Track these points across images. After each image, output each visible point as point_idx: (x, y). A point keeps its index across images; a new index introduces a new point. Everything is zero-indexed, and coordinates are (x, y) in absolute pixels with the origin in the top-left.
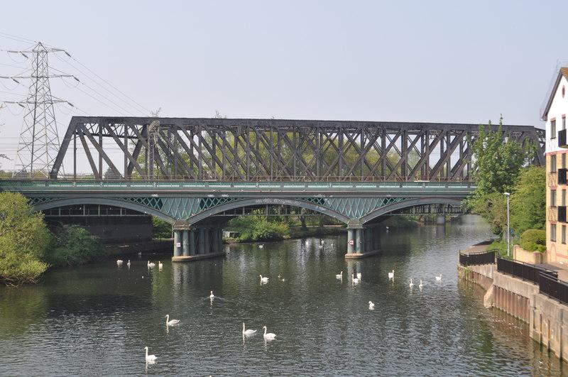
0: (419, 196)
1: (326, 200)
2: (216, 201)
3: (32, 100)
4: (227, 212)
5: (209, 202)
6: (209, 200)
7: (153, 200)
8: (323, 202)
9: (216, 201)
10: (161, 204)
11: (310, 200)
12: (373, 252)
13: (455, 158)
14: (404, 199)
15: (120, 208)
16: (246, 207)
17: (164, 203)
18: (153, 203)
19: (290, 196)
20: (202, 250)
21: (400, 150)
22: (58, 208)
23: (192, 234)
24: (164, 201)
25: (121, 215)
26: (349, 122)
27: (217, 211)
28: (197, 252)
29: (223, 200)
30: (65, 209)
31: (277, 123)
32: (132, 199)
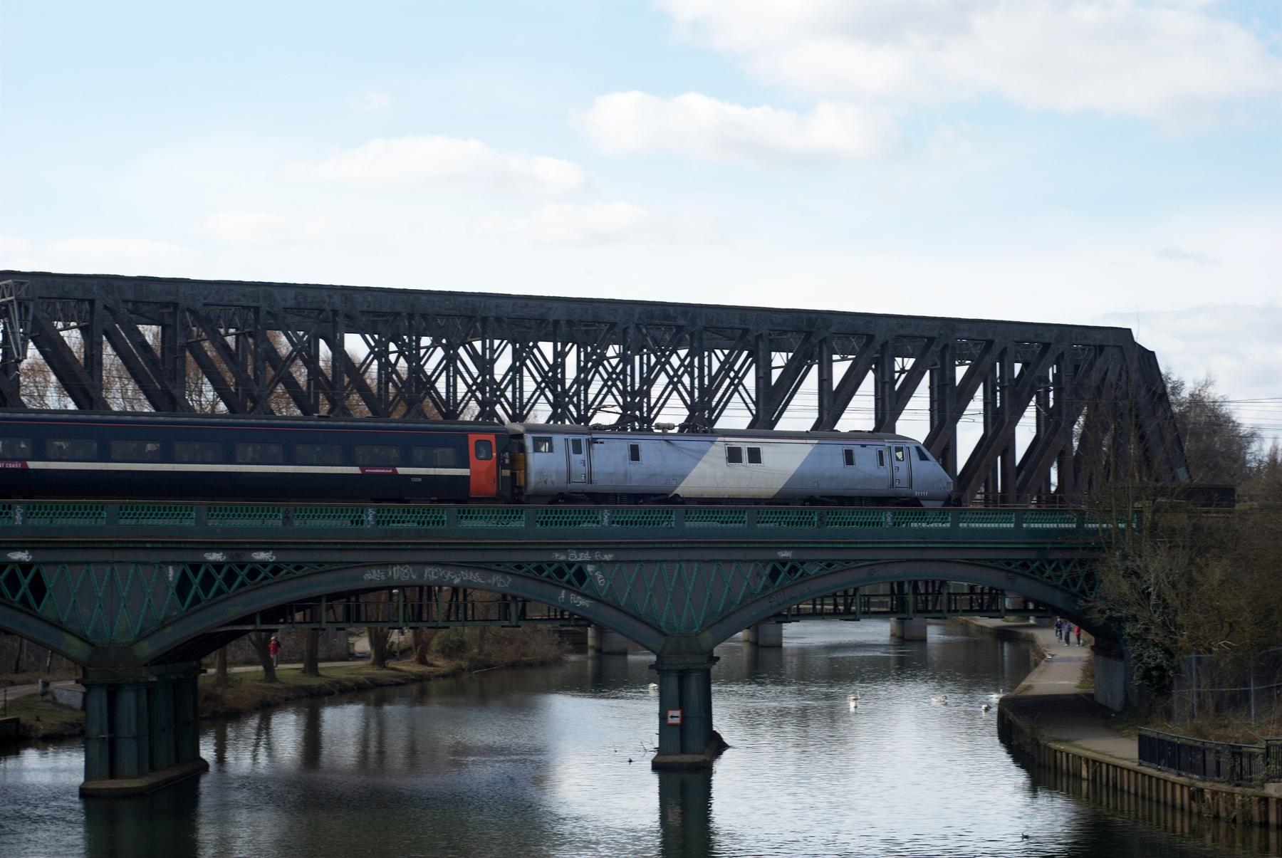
1: (590, 568)
2: (230, 578)
5: (207, 581)
7: (13, 572)
8: (581, 575)
9: (230, 578)
10: (38, 588)
11: (540, 569)
13: (1025, 432)
14: (298, 568)
19: (477, 557)
24: (51, 578)
29: (253, 574)
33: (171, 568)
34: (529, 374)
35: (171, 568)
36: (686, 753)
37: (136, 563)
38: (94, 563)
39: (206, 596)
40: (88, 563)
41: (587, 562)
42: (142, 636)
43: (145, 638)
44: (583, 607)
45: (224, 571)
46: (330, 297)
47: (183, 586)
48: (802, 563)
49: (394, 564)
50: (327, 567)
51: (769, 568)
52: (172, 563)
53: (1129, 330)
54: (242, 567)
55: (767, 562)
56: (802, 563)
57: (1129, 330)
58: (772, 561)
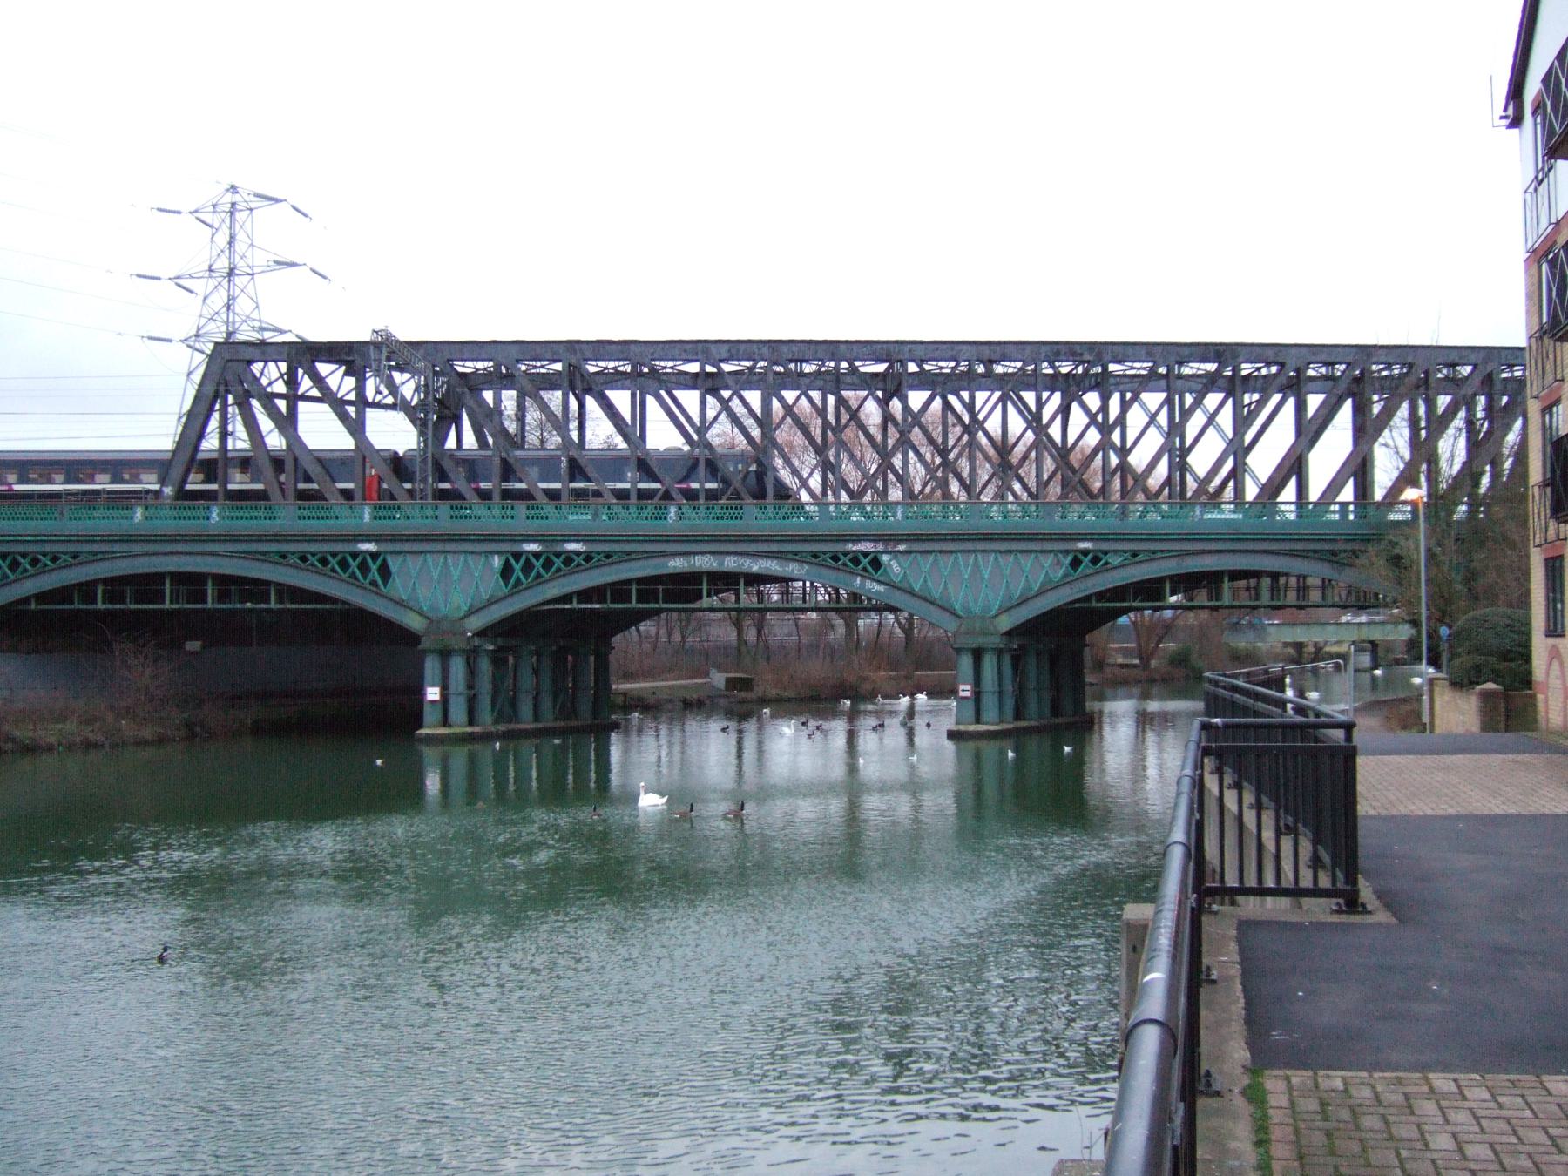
0: (1177, 546)
1: (885, 558)
2: (548, 564)
3: (222, 264)
4: (1100, 596)
5: (527, 568)
6: (528, 561)
7: (364, 560)
8: (876, 564)
9: (548, 564)
10: (385, 572)
12: (469, 729)
14: (1135, 554)
15: (268, 583)
16: (639, 581)
17: (393, 569)
18: (364, 567)
19: (774, 547)
20: (1032, 706)
22: (629, 582)
24: (394, 564)
27: (553, 590)
31: (784, 349)
32: (835, 558)
37: (465, 552)
41: (883, 552)
42: (1004, 610)
44: (878, 592)
47: (506, 571)
51: (1070, 558)
54: (558, 555)
55: (1067, 552)
56: (1106, 553)
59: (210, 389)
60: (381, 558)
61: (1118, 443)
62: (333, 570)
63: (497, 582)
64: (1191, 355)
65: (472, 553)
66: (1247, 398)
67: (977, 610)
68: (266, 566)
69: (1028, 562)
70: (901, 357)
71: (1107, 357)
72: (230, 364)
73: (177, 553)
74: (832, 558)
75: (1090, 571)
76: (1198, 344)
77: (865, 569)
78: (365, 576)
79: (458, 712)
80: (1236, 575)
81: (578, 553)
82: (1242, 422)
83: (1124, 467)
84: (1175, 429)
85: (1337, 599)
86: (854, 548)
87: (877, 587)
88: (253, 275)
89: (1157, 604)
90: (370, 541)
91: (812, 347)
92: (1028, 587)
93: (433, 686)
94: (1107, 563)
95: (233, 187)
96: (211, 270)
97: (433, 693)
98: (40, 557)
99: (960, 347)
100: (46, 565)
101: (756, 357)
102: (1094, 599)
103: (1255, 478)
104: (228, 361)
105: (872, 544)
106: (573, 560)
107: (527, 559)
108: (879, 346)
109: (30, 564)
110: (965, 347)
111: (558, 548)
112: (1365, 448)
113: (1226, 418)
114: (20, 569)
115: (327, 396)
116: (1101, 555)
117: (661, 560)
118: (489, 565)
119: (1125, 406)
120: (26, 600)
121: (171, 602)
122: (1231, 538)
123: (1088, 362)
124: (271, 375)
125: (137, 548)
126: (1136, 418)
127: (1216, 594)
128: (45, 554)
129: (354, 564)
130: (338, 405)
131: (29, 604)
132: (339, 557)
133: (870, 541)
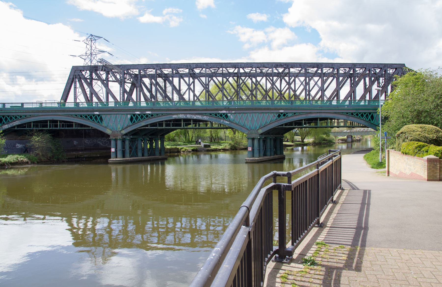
1: (229, 115)
2: (142, 117)
3: (89, 52)
4: (286, 124)
5: (137, 118)
6: (6, 118)
8: (227, 116)
10: (101, 119)
15: (73, 122)
18: (96, 118)
19: (200, 112)
21: (377, 81)
22: (163, 121)
23: (261, 141)
25: (74, 128)
26: (263, 63)
27: (143, 124)
28: (265, 155)
29: (147, 116)
30: (36, 123)
33: (129, 115)
34: (296, 85)
35: (129, 115)
36: (267, 156)
37: (121, 114)
38: (112, 114)
39: (137, 121)
40: (111, 114)
41: (228, 113)
43: (123, 129)
44: (227, 124)
45: (140, 116)
46: (203, 65)
47: (131, 119)
48: (287, 113)
49: (180, 114)
50: (164, 115)
51: (278, 115)
52: (129, 114)
53: (404, 64)
54: (144, 115)
55: (277, 113)
56: (287, 113)
57: (404, 64)
58: (278, 113)
59: (72, 77)
60: (371, 114)
61: (293, 88)
62: (88, 119)
63: (129, 122)
64: (311, 66)
65: (123, 114)
66: (325, 78)
67: (253, 128)
68: (72, 118)
69: (266, 116)
70: (238, 67)
71: (290, 66)
72: (76, 71)
73: (59, 115)
74: (215, 115)
75: (283, 118)
76: (313, 63)
77: (224, 118)
78: (96, 120)
79: (119, 154)
80: (322, 119)
81: (150, 114)
82: (323, 83)
83: (295, 95)
84: (308, 84)
85: (347, 125)
86: (221, 112)
87: (228, 123)
88: (96, 55)
89: (302, 126)
90: (97, 112)
91: (216, 64)
92: (266, 122)
93: (113, 148)
94: (287, 116)
95: (91, 35)
96: (86, 54)
97: (113, 150)
98: (17, 116)
99: (253, 64)
100: (19, 118)
101: (203, 67)
102: (284, 125)
103: (326, 97)
104: (76, 70)
105: (226, 111)
106: (148, 116)
107: (137, 116)
108: (233, 64)
109: (15, 118)
110: (254, 64)
111: (144, 113)
112: (354, 89)
113: (319, 83)
114: (13, 119)
115: (99, 78)
116: (286, 114)
117: (170, 116)
118: (127, 117)
119: (310, 80)
120: (14, 127)
121: (75, 127)
122: (321, 109)
123: (285, 68)
124: (87, 74)
125: (40, 114)
126: (312, 83)
127: (316, 124)
128: (23, 115)
129: (93, 118)
130: (102, 81)
131: (15, 128)
132: (90, 116)
133: (225, 110)
